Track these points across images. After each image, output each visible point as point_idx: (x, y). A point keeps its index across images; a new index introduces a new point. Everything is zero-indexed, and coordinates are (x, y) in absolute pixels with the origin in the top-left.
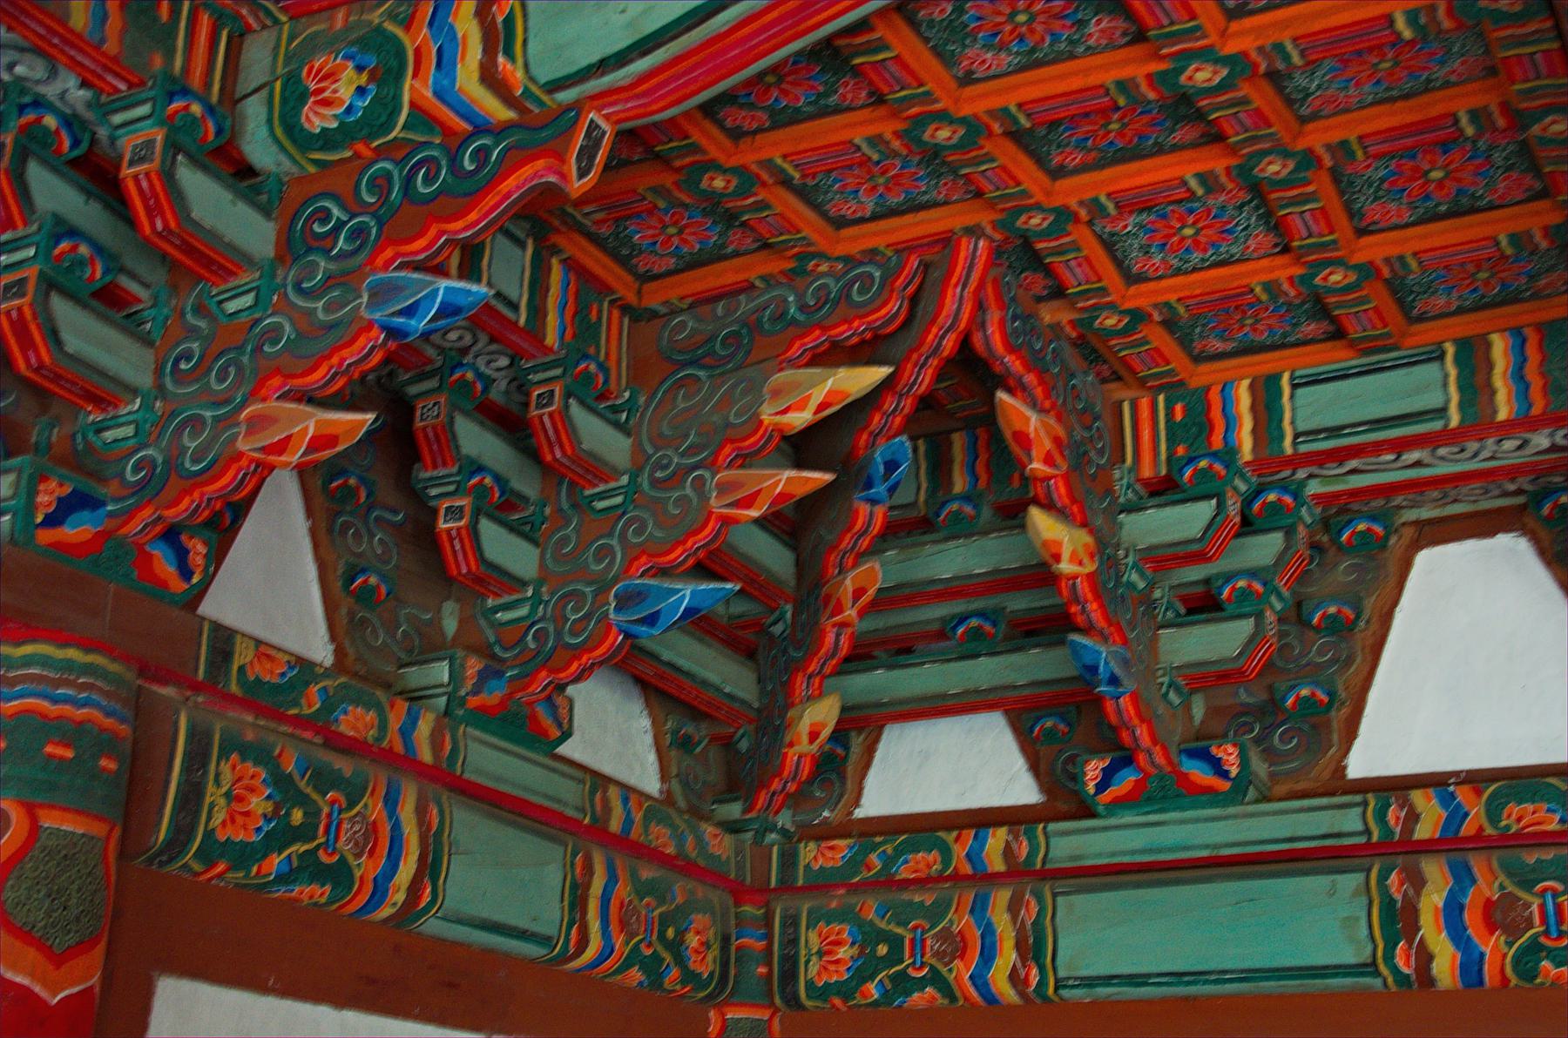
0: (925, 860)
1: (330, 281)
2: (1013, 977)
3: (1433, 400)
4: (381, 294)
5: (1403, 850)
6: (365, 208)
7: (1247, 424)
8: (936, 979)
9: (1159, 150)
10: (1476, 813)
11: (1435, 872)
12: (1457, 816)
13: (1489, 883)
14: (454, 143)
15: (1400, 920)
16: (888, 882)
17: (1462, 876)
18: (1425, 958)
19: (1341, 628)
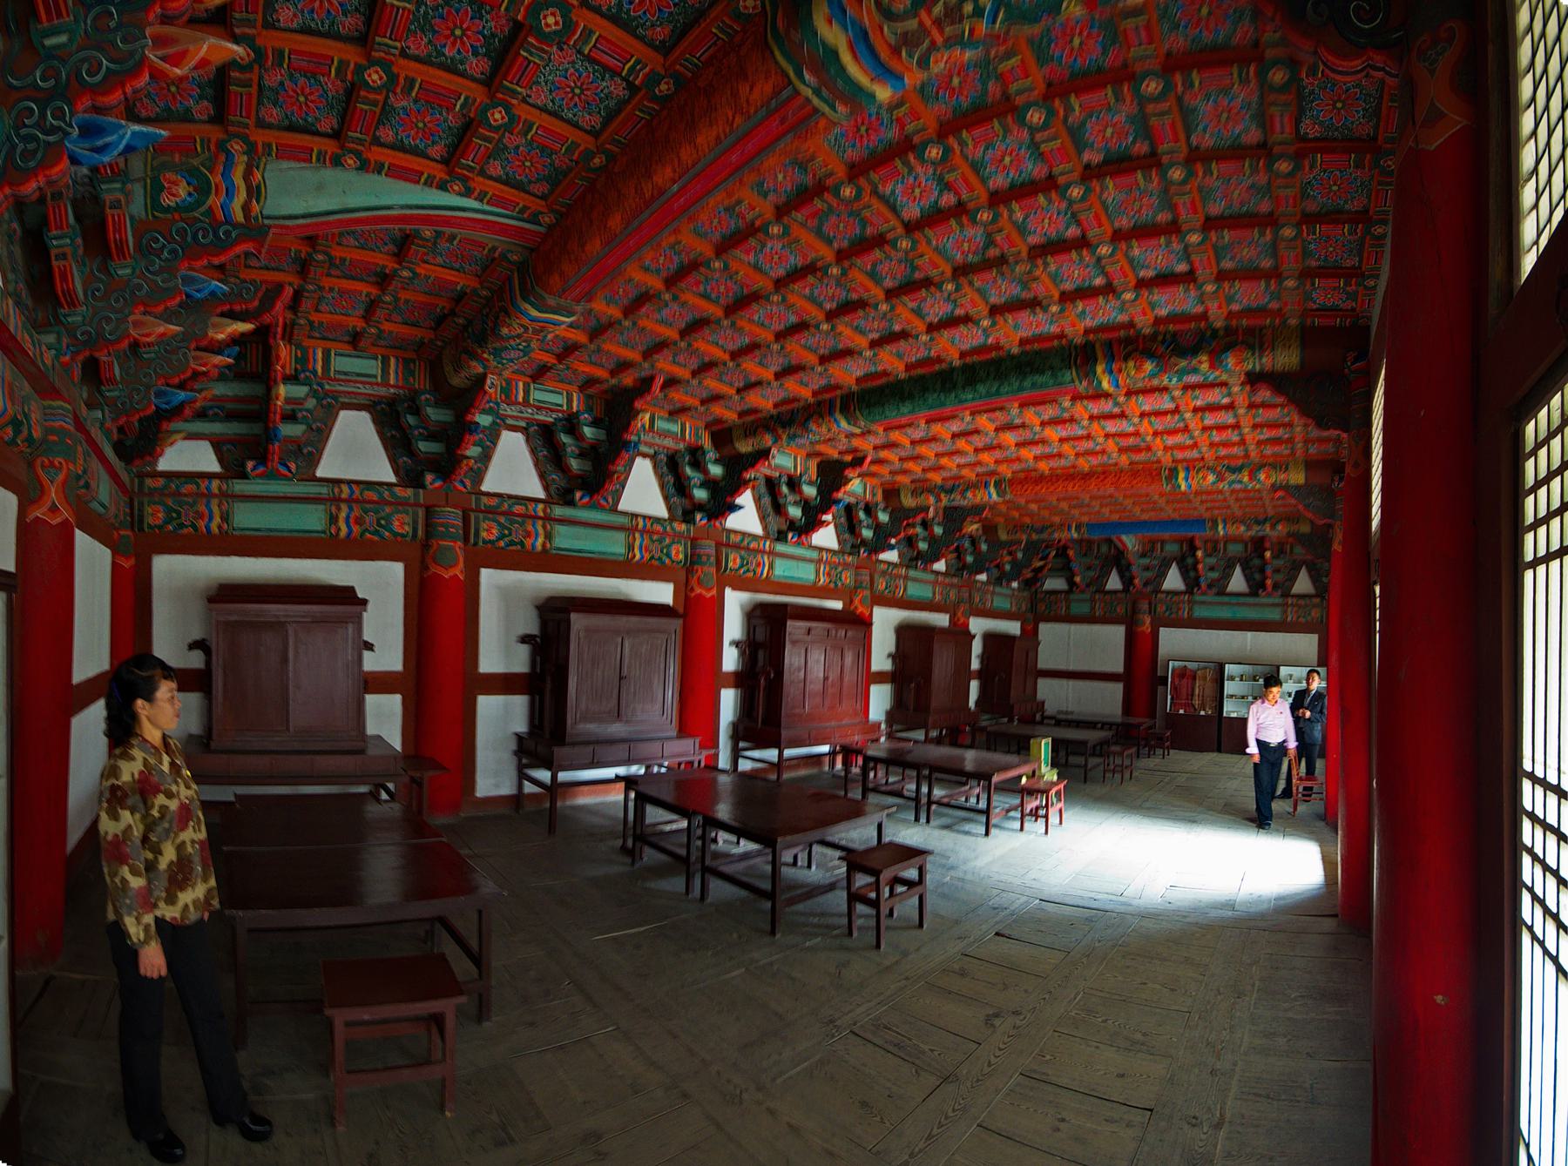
0: (192, 487)
1: (162, 270)
2: (219, 527)
4: (188, 280)
5: (337, 500)
6: (176, 242)
8: (194, 526)
9: (362, 280)
10: (357, 492)
11: (344, 507)
12: (352, 492)
13: (357, 512)
14: (215, 225)
15: (333, 519)
17: (351, 509)
19: (319, 430)
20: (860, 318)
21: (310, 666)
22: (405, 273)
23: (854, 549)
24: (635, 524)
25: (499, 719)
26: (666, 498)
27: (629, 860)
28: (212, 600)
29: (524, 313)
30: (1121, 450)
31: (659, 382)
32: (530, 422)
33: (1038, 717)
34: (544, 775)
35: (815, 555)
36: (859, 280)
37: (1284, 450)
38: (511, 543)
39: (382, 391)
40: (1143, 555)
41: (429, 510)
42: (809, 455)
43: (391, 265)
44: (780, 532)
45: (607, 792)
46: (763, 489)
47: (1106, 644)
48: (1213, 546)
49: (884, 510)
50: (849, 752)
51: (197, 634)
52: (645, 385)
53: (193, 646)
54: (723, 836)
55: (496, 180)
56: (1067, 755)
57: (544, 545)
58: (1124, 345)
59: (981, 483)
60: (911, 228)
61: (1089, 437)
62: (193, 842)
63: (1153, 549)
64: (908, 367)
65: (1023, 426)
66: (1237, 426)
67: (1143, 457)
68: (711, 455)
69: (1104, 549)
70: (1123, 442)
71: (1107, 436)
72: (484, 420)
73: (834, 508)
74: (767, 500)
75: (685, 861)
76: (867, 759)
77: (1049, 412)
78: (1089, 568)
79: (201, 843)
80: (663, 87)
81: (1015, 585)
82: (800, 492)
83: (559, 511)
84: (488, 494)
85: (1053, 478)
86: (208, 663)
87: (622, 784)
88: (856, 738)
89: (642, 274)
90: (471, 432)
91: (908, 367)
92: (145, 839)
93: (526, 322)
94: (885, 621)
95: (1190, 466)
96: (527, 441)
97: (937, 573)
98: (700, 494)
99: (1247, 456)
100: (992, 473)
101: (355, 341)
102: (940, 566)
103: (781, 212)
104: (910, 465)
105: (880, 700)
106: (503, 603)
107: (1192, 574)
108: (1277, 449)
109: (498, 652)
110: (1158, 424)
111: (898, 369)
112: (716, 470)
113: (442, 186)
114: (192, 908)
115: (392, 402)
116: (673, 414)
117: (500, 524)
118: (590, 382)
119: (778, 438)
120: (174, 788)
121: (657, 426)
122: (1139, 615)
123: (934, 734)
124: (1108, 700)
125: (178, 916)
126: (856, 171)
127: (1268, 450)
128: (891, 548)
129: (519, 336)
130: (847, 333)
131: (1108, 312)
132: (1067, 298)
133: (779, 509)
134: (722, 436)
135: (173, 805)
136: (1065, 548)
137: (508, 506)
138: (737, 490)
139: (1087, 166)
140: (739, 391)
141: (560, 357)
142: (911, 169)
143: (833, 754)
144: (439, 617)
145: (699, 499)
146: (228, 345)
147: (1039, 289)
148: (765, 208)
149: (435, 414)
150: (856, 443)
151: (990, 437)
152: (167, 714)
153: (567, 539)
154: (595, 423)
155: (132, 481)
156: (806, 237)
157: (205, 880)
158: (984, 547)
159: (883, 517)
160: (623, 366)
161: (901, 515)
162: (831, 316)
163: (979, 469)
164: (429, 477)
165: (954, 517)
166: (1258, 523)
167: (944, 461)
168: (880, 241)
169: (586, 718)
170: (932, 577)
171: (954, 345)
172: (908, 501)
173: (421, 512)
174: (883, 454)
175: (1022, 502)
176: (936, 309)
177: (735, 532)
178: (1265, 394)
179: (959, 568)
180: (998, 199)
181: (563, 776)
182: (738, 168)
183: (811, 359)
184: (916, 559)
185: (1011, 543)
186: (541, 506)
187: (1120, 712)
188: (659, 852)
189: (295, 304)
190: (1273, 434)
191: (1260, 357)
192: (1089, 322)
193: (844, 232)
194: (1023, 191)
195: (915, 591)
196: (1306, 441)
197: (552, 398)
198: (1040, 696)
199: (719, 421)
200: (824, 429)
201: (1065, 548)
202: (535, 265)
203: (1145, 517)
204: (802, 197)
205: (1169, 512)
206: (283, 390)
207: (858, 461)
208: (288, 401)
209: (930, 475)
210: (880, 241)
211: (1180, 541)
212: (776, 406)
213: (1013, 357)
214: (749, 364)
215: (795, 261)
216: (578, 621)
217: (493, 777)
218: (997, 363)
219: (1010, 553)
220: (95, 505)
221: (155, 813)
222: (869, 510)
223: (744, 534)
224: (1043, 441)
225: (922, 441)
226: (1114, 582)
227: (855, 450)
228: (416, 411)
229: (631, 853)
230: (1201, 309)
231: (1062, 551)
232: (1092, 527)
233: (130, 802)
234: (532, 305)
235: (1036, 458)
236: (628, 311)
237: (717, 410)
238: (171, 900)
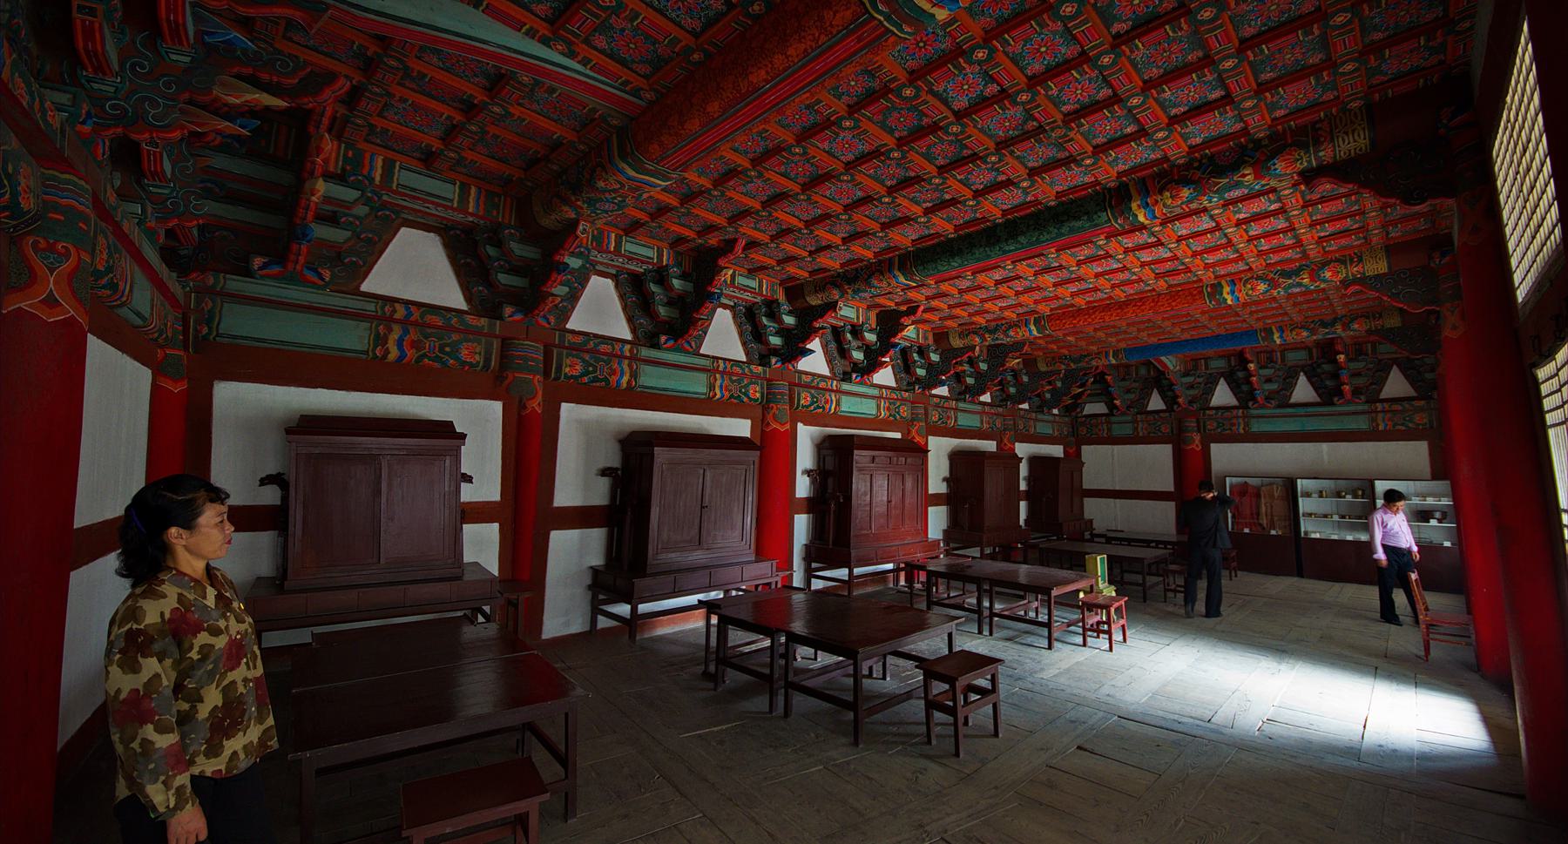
3: (450, 196)
7: (379, 171)
13: (414, 335)
15: (381, 340)
17: (406, 331)
18: (387, 352)
20: (915, 192)
21: (405, 505)
22: (496, 109)
23: (910, 386)
24: (715, 367)
25: (572, 553)
26: (744, 344)
27: (711, 685)
28: (289, 431)
29: (622, 172)
30: (1158, 276)
31: (742, 243)
32: (620, 270)
33: (1087, 535)
34: (624, 609)
35: (875, 392)
36: (917, 163)
37: (1355, 241)
38: (596, 380)
39: (459, 217)
40: (1186, 374)
41: (506, 343)
42: (869, 307)
43: (480, 97)
44: (845, 373)
45: (686, 620)
46: (830, 337)
47: (1153, 464)
48: (1267, 358)
49: (935, 352)
50: (911, 569)
51: (271, 469)
52: (729, 245)
53: (264, 481)
54: (803, 652)
55: (600, 52)
56: (1122, 572)
57: (629, 382)
58: (1158, 179)
59: (1022, 322)
60: (959, 116)
61: (1124, 269)
62: (246, 680)
63: (1196, 368)
64: (957, 228)
65: (1061, 267)
66: (1291, 229)
67: (1181, 279)
68: (785, 307)
69: (1143, 371)
70: (1159, 269)
71: (1143, 265)
72: (575, 263)
73: (892, 352)
74: (833, 345)
75: (768, 679)
76: (930, 574)
77: (1086, 252)
78: (1128, 391)
79: (256, 680)
80: (756, 7)
81: (1055, 411)
82: (863, 338)
83: (645, 352)
84: (573, 332)
85: (1091, 309)
86: (285, 498)
87: (703, 611)
88: (919, 556)
89: (733, 153)
90: (559, 272)
91: (957, 228)
92: (178, 688)
93: (622, 179)
94: (939, 449)
95: (1234, 280)
96: (617, 286)
97: (984, 404)
98: (775, 341)
99: (1305, 255)
100: (1034, 312)
101: (428, 161)
102: (986, 398)
103: (853, 109)
104: (957, 311)
105: (937, 521)
106: (583, 435)
107: (1245, 388)
108: (1344, 242)
109: (573, 484)
110: (1196, 245)
111: (949, 231)
112: (789, 320)
113: (544, 41)
114: (242, 756)
115: (469, 230)
116: (752, 272)
117: (584, 361)
118: (680, 241)
119: (844, 293)
120: (222, 624)
121: (738, 282)
122: (1188, 433)
123: (988, 551)
124: (1161, 519)
125: (223, 767)
126: (915, 76)
127: (1332, 246)
128: (942, 383)
129: (615, 191)
130: (905, 204)
131: (1142, 153)
132: (1099, 150)
133: (844, 353)
134: (794, 291)
135: (220, 642)
136: (1103, 374)
137: (591, 344)
138: (808, 337)
139: (1118, 36)
140: (811, 253)
141: (653, 216)
142: (961, 69)
143: (896, 571)
144: (528, 451)
145: (773, 345)
146: (242, 115)
147: (1074, 148)
148: (840, 106)
149: (518, 249)
150: (911, 295)
151: (1030, 280)
152: (209, 546)
153: (652, 378)
154: (684, 276)
155: (187, 296)
156: (873, 129)
157: (260, 720)
158: (1025, 379)
159: (935, 357)
160: (711, 228)
161: (949, 354)
162: (891, 191)
163: (1021, 310)
164: (508, 310)
165: (997, 354)
166: (1324, 324)
167: (988, 305)
168: (934, 128)
169: (666, 549)
170: (979, 408)
171: (996, 207)
172: (957, 343)
173: (496, 344)
174: (934, 303)
175: (1060, 334)
176: (981, 178)
177: (806, 373)
178: (1326, 187)
179: (1003, 399)
180: (1035, 81)
181: (643, 608)
182: (820, 76)
183: (874, 226)
184: (964, 392)
185: (1052, 373)
186: (627, 347)
187: (1174, 531)
188: (737, 678)
189: (353, 98)
190: (1338, 226)
191: (1316, 152)
192: (1122, 167)
193: (903, 123)
194: (1058, 70)
195: (965, 421)
196: (1385, 226)
197: (643, 251)
198: (1087, 516)
199: (793, 279)
200: (884, 284)
201: (1103, 374)
202: (639, 131)
203: (1186, 336)
204: (870, 98)
205: (1214, 328)
206: (321, 186)
207: (912, 311)
208: (327, 200)
209: (976, 319)
210: (934, 128)
211: (1226, 356)
212: (842, 265)
213: (1049, 208)
214: (821, 232)
215: (863, 148)
216: (661, 454)
217: (562, 613)
218: (1035, 217)
219: (1050, 383)
220: (124, 312)
221: (194, 655)
222: (922, 352)
223: (813, 375)
224: (1080, 279)
225: (969, 290)
226: (1156, 403)
227: (910, 301)
228: (499, 244)
229: (714, 678)
230: (1240, 126)
231: (1100, 378)
232: (1130, 351)
233: (156, 647)
234: (630, 166)
235: (1073, 295)
236: (717, 183)
237: (791, 269)
238: (213, 751)
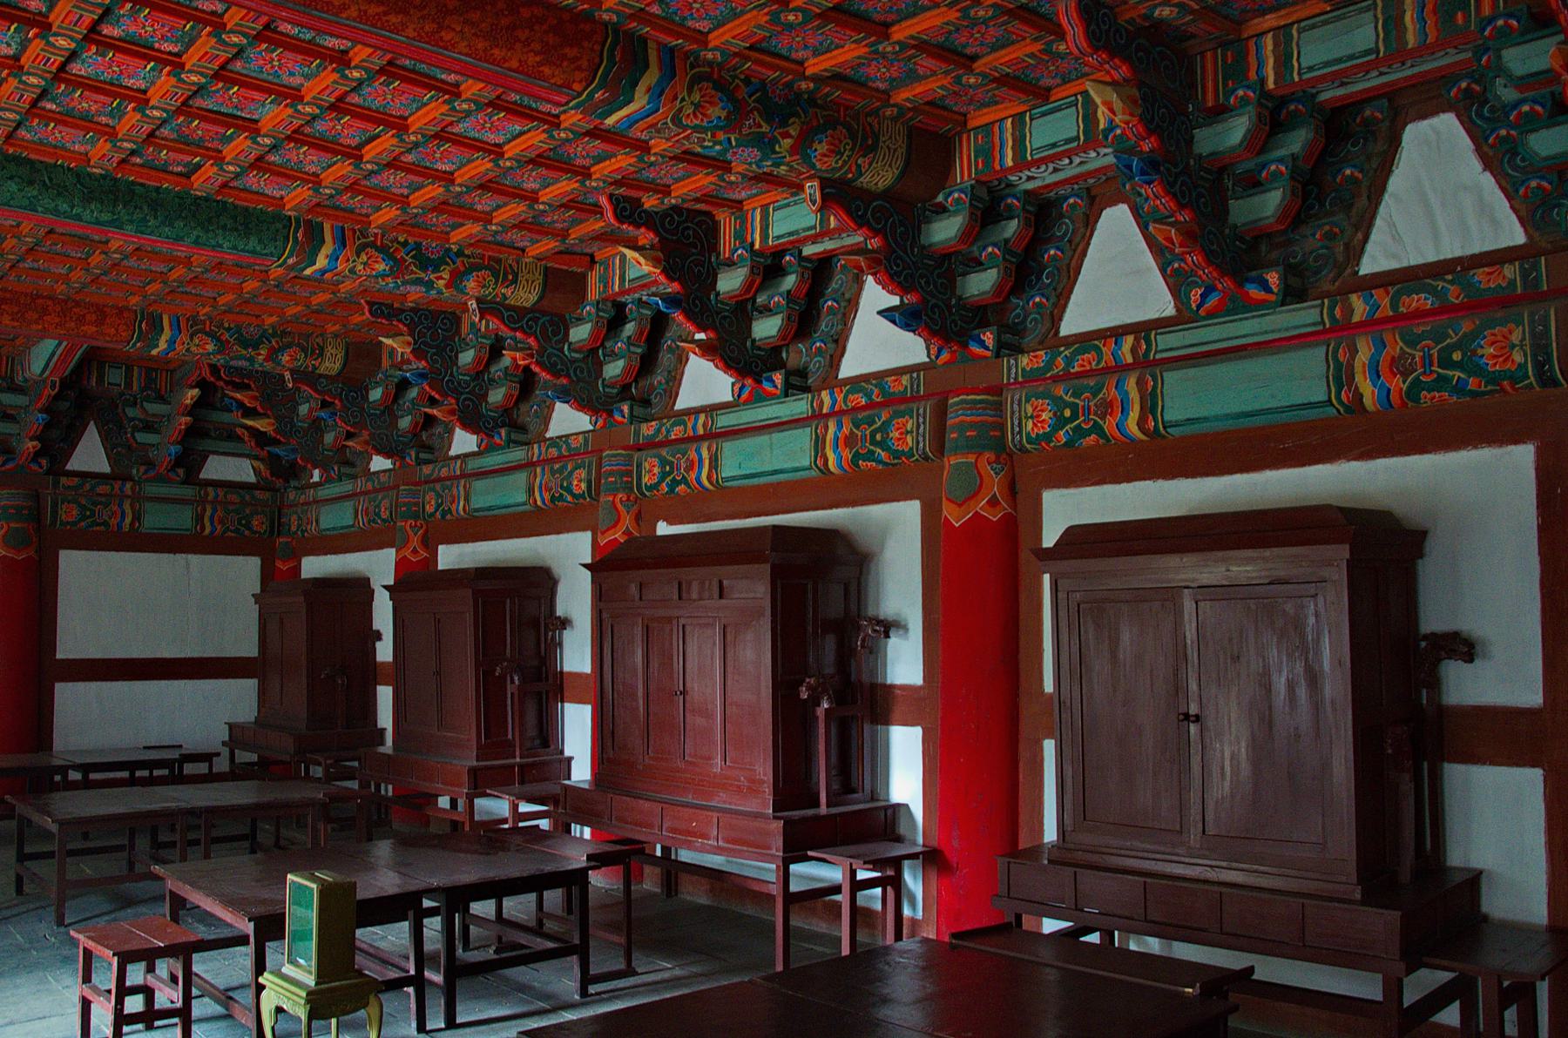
8: (1097, 428)
15: (199, 519)
16: (1066, 376)
47: (217, 598)
